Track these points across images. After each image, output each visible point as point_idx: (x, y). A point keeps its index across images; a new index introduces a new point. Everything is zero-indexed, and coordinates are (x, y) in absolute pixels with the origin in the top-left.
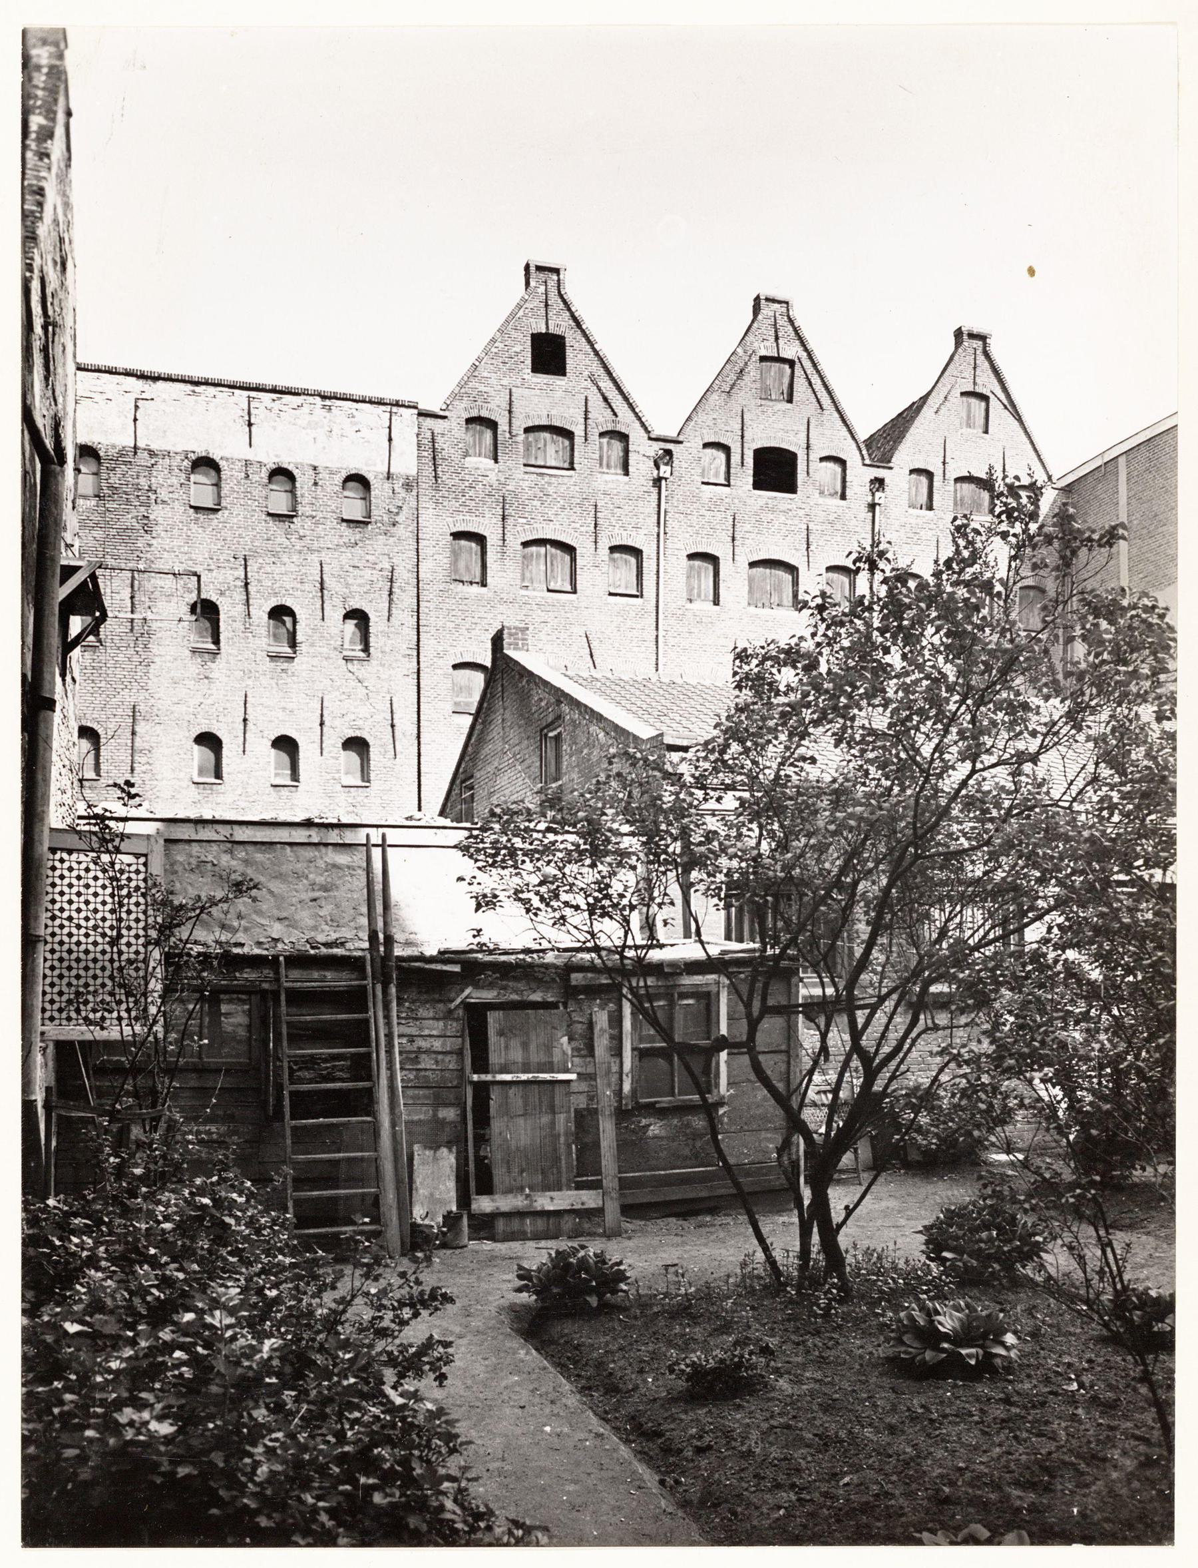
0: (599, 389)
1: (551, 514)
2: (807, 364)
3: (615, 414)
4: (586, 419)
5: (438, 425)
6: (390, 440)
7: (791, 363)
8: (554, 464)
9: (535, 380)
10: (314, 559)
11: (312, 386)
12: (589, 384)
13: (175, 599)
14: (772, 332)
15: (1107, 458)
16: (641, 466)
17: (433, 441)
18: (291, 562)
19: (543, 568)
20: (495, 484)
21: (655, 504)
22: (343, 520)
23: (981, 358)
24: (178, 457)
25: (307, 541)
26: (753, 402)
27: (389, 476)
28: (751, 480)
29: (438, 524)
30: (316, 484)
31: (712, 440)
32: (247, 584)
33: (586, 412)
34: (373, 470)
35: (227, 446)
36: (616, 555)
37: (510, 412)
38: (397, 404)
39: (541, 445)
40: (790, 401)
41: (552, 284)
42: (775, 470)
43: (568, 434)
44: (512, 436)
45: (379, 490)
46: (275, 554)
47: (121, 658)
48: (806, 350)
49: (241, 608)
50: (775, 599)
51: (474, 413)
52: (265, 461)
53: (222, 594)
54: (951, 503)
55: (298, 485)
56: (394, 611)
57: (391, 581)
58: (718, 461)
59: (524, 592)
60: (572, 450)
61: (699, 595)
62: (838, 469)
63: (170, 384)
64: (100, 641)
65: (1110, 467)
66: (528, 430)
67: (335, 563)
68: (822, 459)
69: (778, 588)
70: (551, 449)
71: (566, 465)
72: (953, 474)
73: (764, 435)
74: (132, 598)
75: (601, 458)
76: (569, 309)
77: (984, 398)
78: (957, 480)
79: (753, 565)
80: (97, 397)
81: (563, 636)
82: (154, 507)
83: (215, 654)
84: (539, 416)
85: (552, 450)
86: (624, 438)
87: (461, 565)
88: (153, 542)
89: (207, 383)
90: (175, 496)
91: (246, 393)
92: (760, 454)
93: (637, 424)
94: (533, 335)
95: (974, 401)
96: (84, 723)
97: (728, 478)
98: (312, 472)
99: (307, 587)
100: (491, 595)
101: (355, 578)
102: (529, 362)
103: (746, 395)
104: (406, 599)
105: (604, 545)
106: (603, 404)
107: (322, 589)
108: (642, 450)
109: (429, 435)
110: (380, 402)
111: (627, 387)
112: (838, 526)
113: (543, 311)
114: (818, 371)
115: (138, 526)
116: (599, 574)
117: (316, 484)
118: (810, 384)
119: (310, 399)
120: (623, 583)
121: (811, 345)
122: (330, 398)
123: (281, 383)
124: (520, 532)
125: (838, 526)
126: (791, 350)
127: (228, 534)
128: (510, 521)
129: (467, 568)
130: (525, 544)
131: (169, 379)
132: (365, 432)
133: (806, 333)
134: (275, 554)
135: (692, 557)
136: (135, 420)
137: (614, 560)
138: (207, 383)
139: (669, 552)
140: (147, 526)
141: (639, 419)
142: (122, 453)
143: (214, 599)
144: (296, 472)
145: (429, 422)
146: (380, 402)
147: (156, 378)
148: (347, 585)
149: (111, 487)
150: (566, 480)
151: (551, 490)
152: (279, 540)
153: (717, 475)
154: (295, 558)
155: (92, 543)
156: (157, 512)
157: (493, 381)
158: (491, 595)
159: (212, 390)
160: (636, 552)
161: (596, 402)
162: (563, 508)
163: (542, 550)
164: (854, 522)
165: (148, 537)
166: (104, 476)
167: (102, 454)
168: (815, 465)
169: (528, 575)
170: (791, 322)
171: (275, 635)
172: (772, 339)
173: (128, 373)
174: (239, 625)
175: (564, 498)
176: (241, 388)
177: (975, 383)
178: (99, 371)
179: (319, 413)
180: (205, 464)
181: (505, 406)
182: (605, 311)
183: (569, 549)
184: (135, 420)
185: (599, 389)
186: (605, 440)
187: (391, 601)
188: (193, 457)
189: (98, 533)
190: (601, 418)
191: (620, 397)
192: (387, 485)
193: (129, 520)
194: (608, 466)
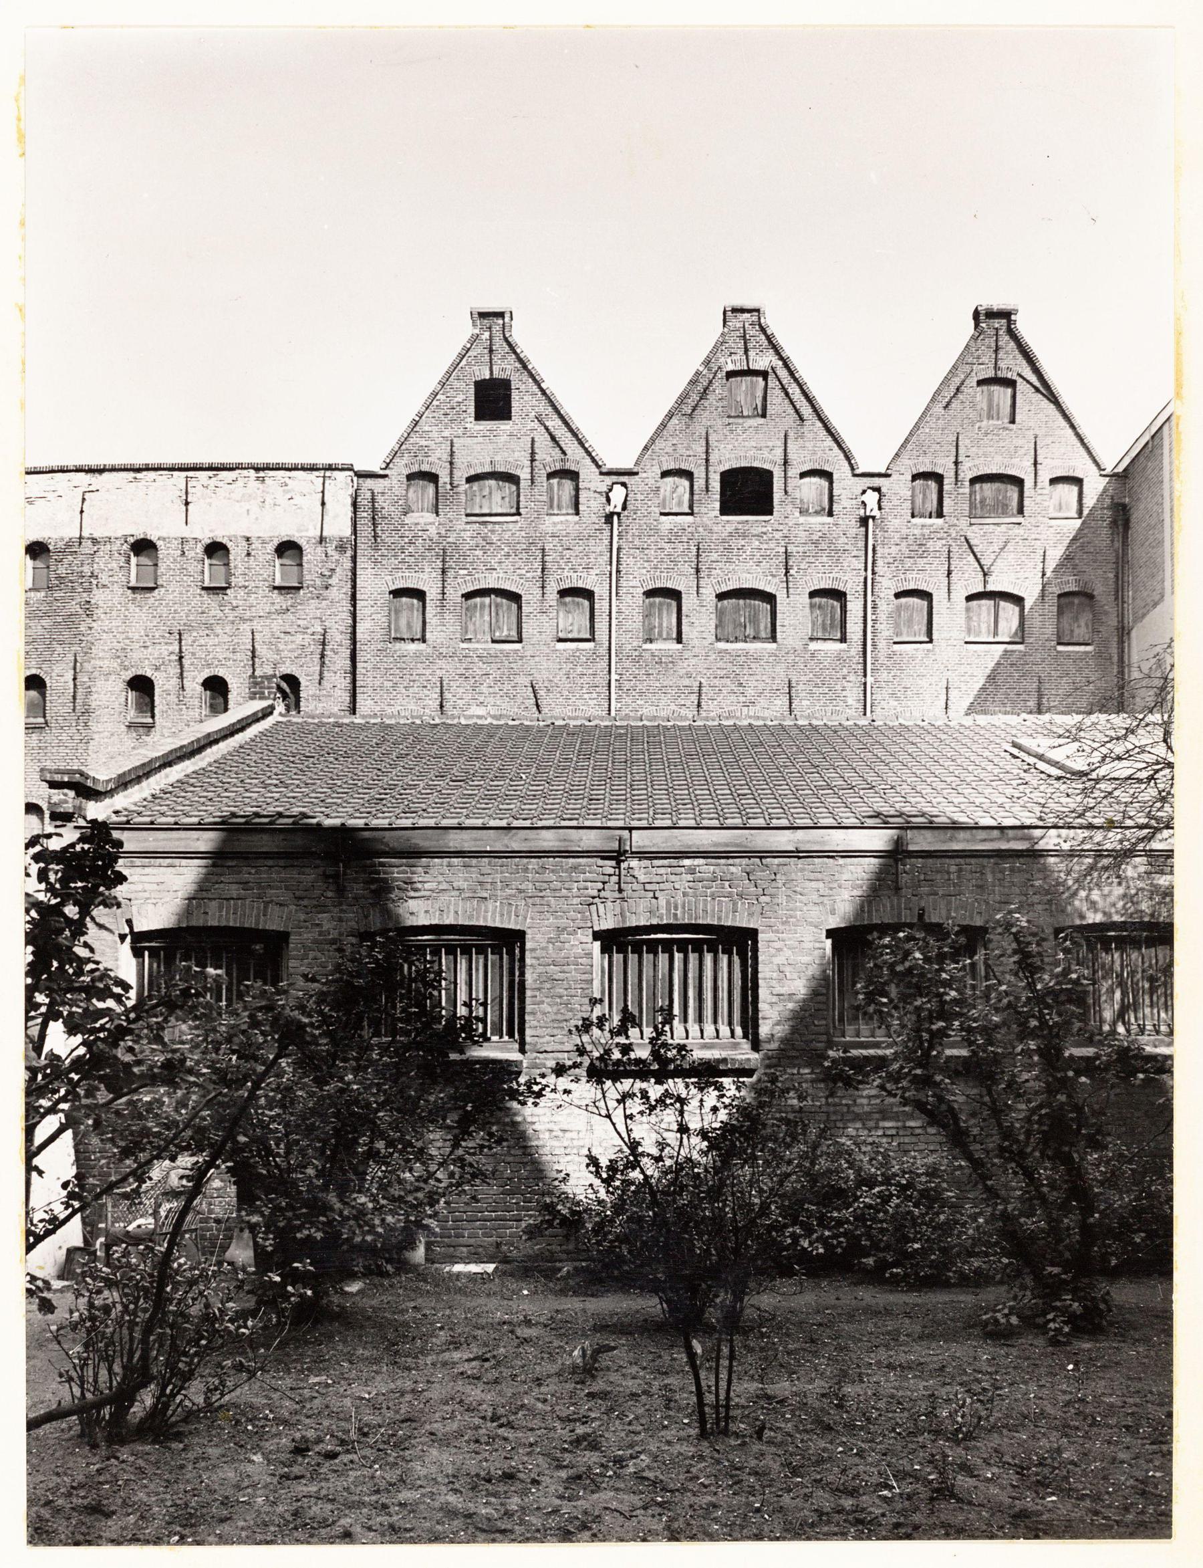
0: (547, 429)
1: (494, 563)
2: (783, 373)
3: (564, 453)
4: (533, 460)
5: (377, 485)
6: (323, 504)
7: (764, 374)
8: (500, 511)
9: (478, 428)
10: (246, 628)
11: (245, 460)
12: (536, 424)
13: (113, 677)
14: (741, 345)
15: (1154, 430)
16: (592, 505)
17: (373, 500)
18: (223, 632)
19: (487, 618)
20: (436, 537)
21: (607, 542)
22: (275, 588)
23: (1005, 339)
24: (118, 542)
25: (240, 611)
26: (719, 422)
27: (322, 540)
28: (717, 505)
29: (375, 584)
30: (249, 554)
31: (672, 466)
32: (181, 658)
33: (533, 453)
34: (304, 534)
35: (162, 524)
36: (568, 599)
37: (451, 463)
38: (330, 468)
39: (486, 492)
40: (764, 416)
41: (496, 329)
42: (747, 492)
43: (513, 479)
44: (453, 486)
45: (312, 555)
46: (209, 627)
47: (64, 737)
48: (781, 358)
49: (175, 681)
50: (750, 631)
51: (415, 469)
52: (200, 537)
53: (157, 669)
54: (966, 507)
55: (231, 557)
56: (326, 674)
57: (324, 644)
58: (680, 489)
59: (465, 645)
60: (518, 496)
61: (660, 634)
62: (825, 484)
63: (115, 474)
64: (46, 723)
65: (1157, 440)
66: (470, 480)
67: (266, 631)
68: (803, 475)
69: (754, 620)
70: (497, 497)
71: (514, 511)
72: (967, 474)
73: (729, 456)
74: (75, 679)
75: (551, 499)
76: (515, 352)
77: (1011, 383)
78: (974, 481)
79: (721, 596)
80: (50, 496)
81: (506, 687)
82: (95, 591)
83: (149, 727)
84: (482, 464)
85: (497, 497)
86: (573, 476)
87: (403, 622)
88: (94, 624)
89: (147, 468)
90: (115, 579)
91: (184, 474)
92: (729, 477)
93: (588, 461)
94: (476, 383)
95: (996, 389)
96: (30, 801)
97: (691, 507)
98: (245, 543)
99: (238, 656)
100: (430, 650)
101: (286, 643)
102: (472, 410)
103: (709, 417)
104: (341, 661)
105: (553, 588)
106: (551, 444)
107: (253, 657)
108: (593, 486)
109: (368, 495)
110: (313, 468)
111: (577, 422)
112: (823, 546)
113: (487, 358)
114: (796, 380)
115: (81, 611)
116: (545, 620)
117: (249, 554)
118: (787, 394)
119: (245, 472)
120: (575, 628)
121: (788, 352)
122: (263, 469)
123: (217, 460)
124: (461, 583)
125: (823, 546)
126: (763, 360)
127: (163, 611)
128: (451, 574)
129: (409, 626)
130: (468, 596)
131: (113, 469)
132: (298, 500)
133: (781, 339)
134: (209, 627)
135: (650, 594)
136: (82, 512)
137: (565, 604)
138: (147, 468)
139: (622, 591)
140: (88, 609)
141: (589, 453)
142: (69, 544)
143: (149, 674)
144: (229, 545)
145: (369, 483)
146: (313, 468)
147: (100, 471)
148: (278, 651)
149: (59, 578)
150: (511, 526)
151: (494, 538)
152: (213, 613)
153: (680, 503)
154: (228, 629)
155: (40, 631)
156: (98, 596)
157: (435, 435)
158: (430, 650)
159: (152, 475)
160: (588, 594)
161: (543, 440)
162: (508, 555)
163: (487, 600)
164: (843, 539)
165: (89, 620)
166: (53, 568)
167: (51, 547)
168: (794, 482)
169: (471, 627)
170: (763, 330)
171: (211, 706)
172: (741, 352)
173: (78, 470)
174: (173, 698)
175: (508, 544)
176: (180, 469)
177: (996, 368)
178: (52, 471)
179: (253, 484)
180: (143, 547)
181: (446, 457)
182: (545, 346)
183: (515, 597)
184: (82, 512)
185: (547, 429)
186: (555, 481)
187: (323, 664)
188: (132, 540)
189: (46, 622)
190: (548, 457)
191: (569, 435)
192: (320, 549)
193: (73, 607)
194: (559, 508)
